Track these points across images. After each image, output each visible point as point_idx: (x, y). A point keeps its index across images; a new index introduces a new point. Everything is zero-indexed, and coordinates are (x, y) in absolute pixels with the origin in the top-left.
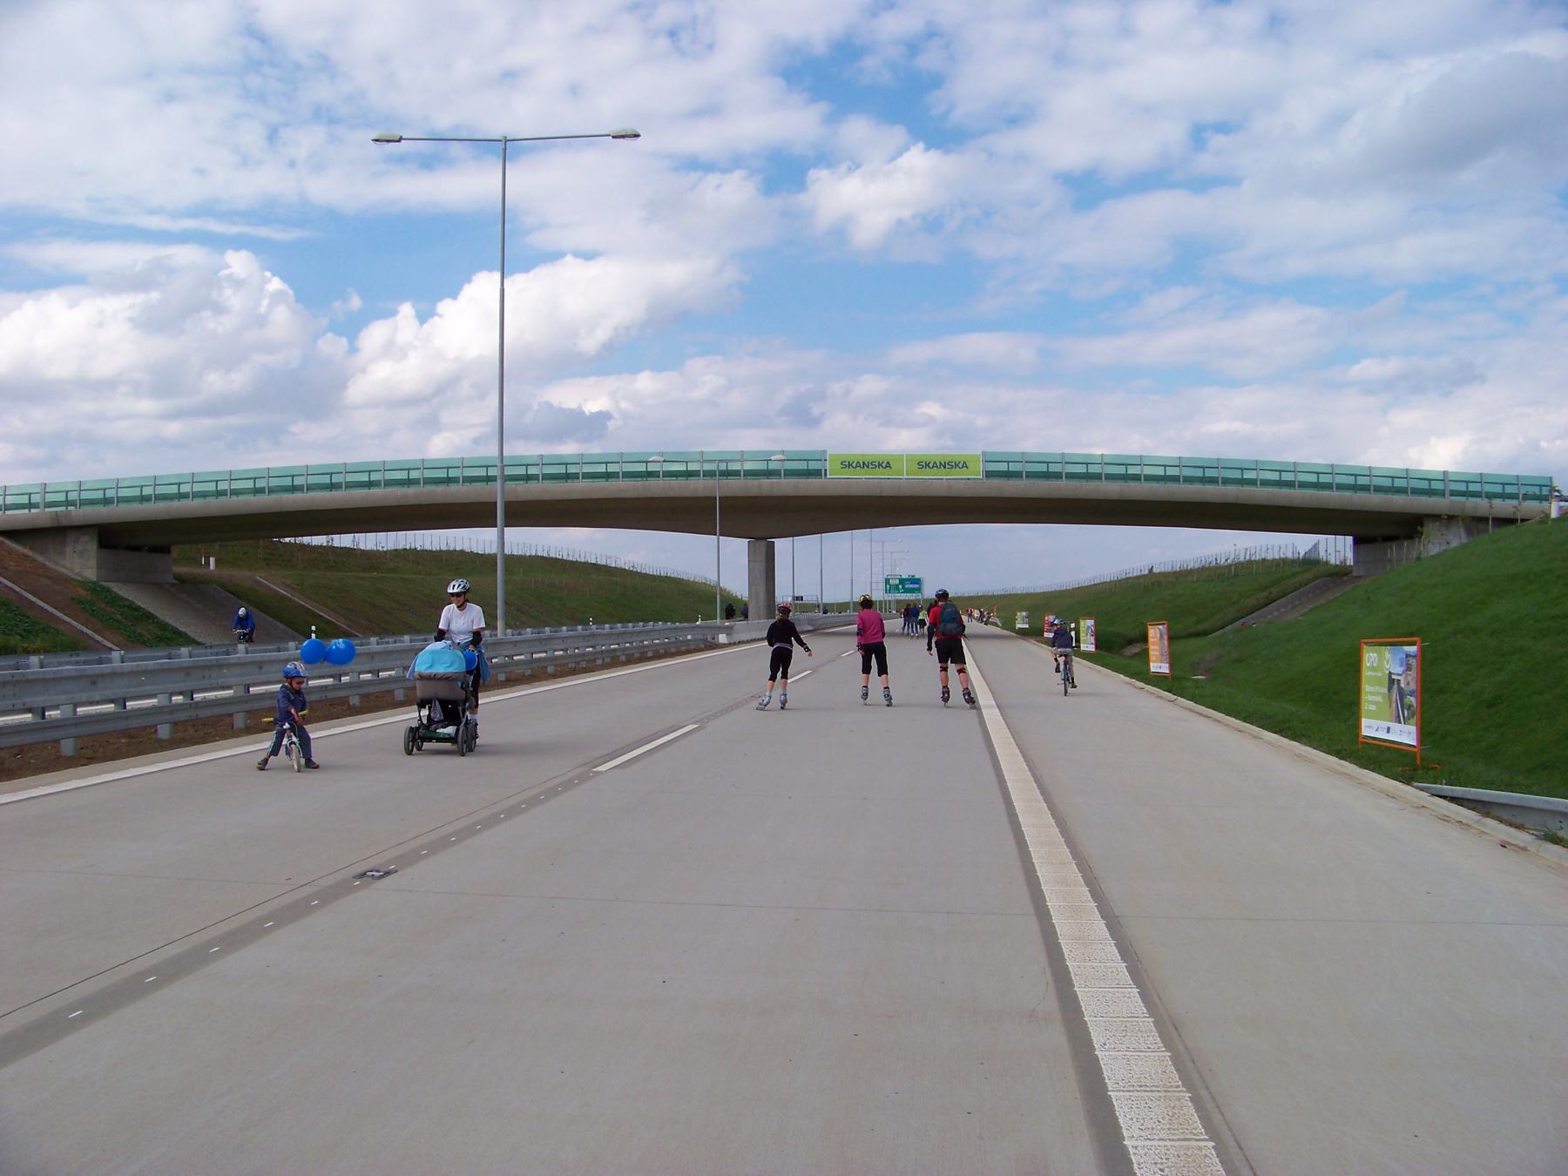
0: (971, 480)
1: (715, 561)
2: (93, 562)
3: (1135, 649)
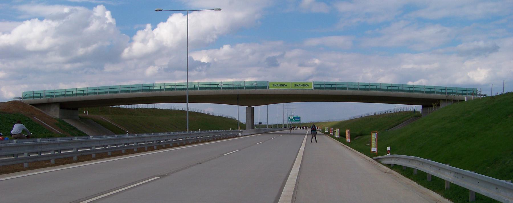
0: (309, 90)
1: (237, 112)
2: (58, 113)
3: (367, 136)
